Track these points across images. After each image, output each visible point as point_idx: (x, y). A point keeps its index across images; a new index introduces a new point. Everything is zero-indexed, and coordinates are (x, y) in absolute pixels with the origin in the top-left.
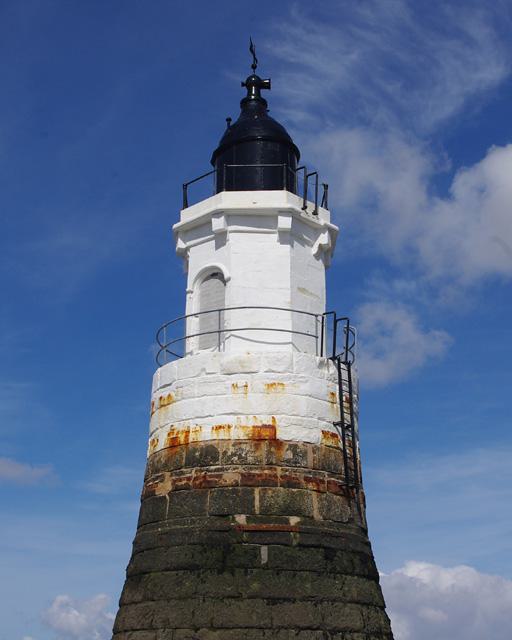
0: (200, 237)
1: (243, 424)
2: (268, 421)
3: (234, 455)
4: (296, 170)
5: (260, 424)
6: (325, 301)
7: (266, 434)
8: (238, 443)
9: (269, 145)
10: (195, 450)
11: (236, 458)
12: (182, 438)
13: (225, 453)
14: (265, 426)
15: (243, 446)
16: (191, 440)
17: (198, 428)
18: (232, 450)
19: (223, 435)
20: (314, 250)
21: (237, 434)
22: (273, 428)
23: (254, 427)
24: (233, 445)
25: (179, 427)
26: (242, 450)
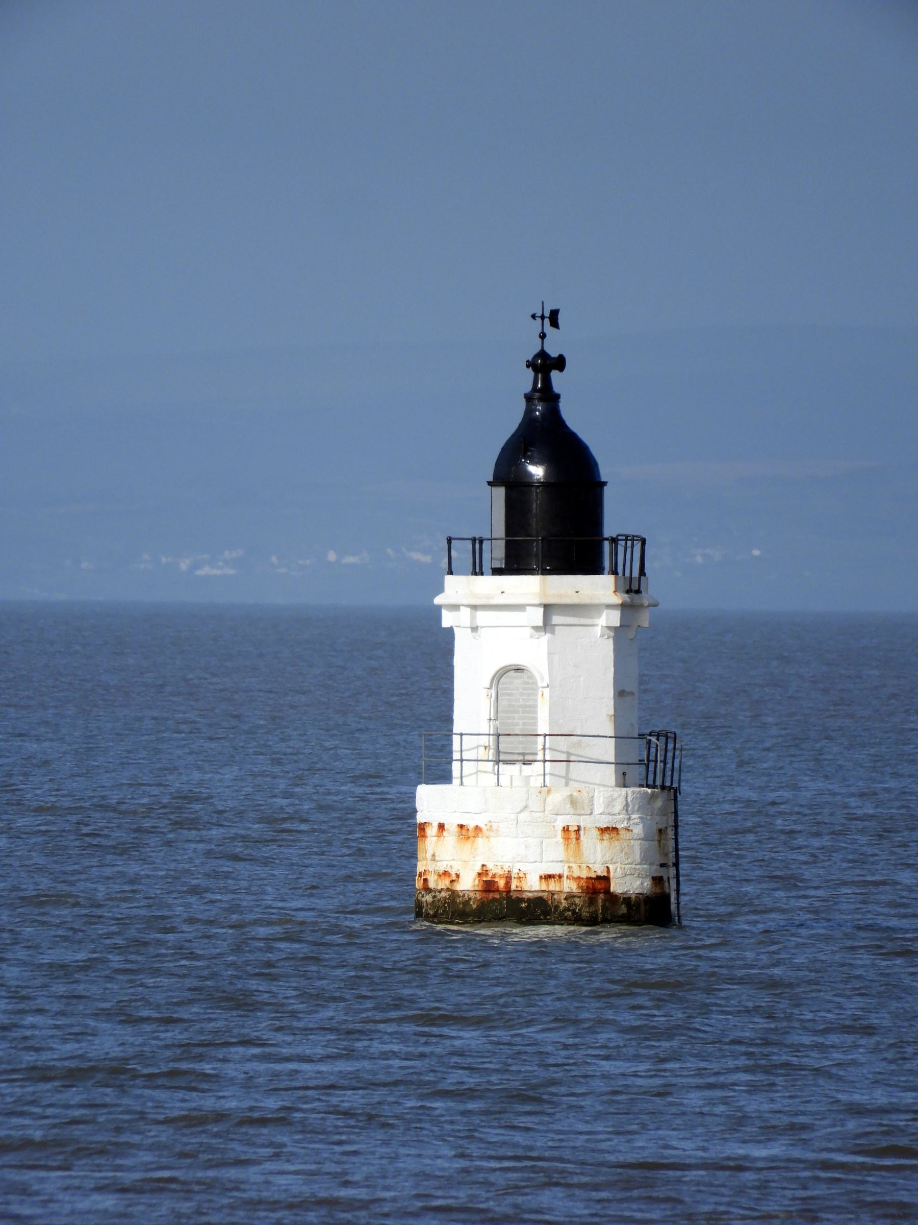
0: (907, 1158)
1: (576, 875)
2: (601, 872)
3: (568, 909)
4: (508, 891)
5: (594, 876)
6: (612, 669)
7: (599, 886)
8: (570, 896)
9: (574, 1017)
10: (522, 900)
11: (570, 913)
12: (501, 883)
13: (557, 907)
14: (599, 878)
15: (577, 900)
16: (513, 887)
17: (521, 875)
18: (564, 904)
19: (553, 886)
20: (598, 631)
21: (569, 886)
22: (606, 879)
23: (587, 878)
24: (566, 899)
25: (496, 868)
26: (576, 905)
